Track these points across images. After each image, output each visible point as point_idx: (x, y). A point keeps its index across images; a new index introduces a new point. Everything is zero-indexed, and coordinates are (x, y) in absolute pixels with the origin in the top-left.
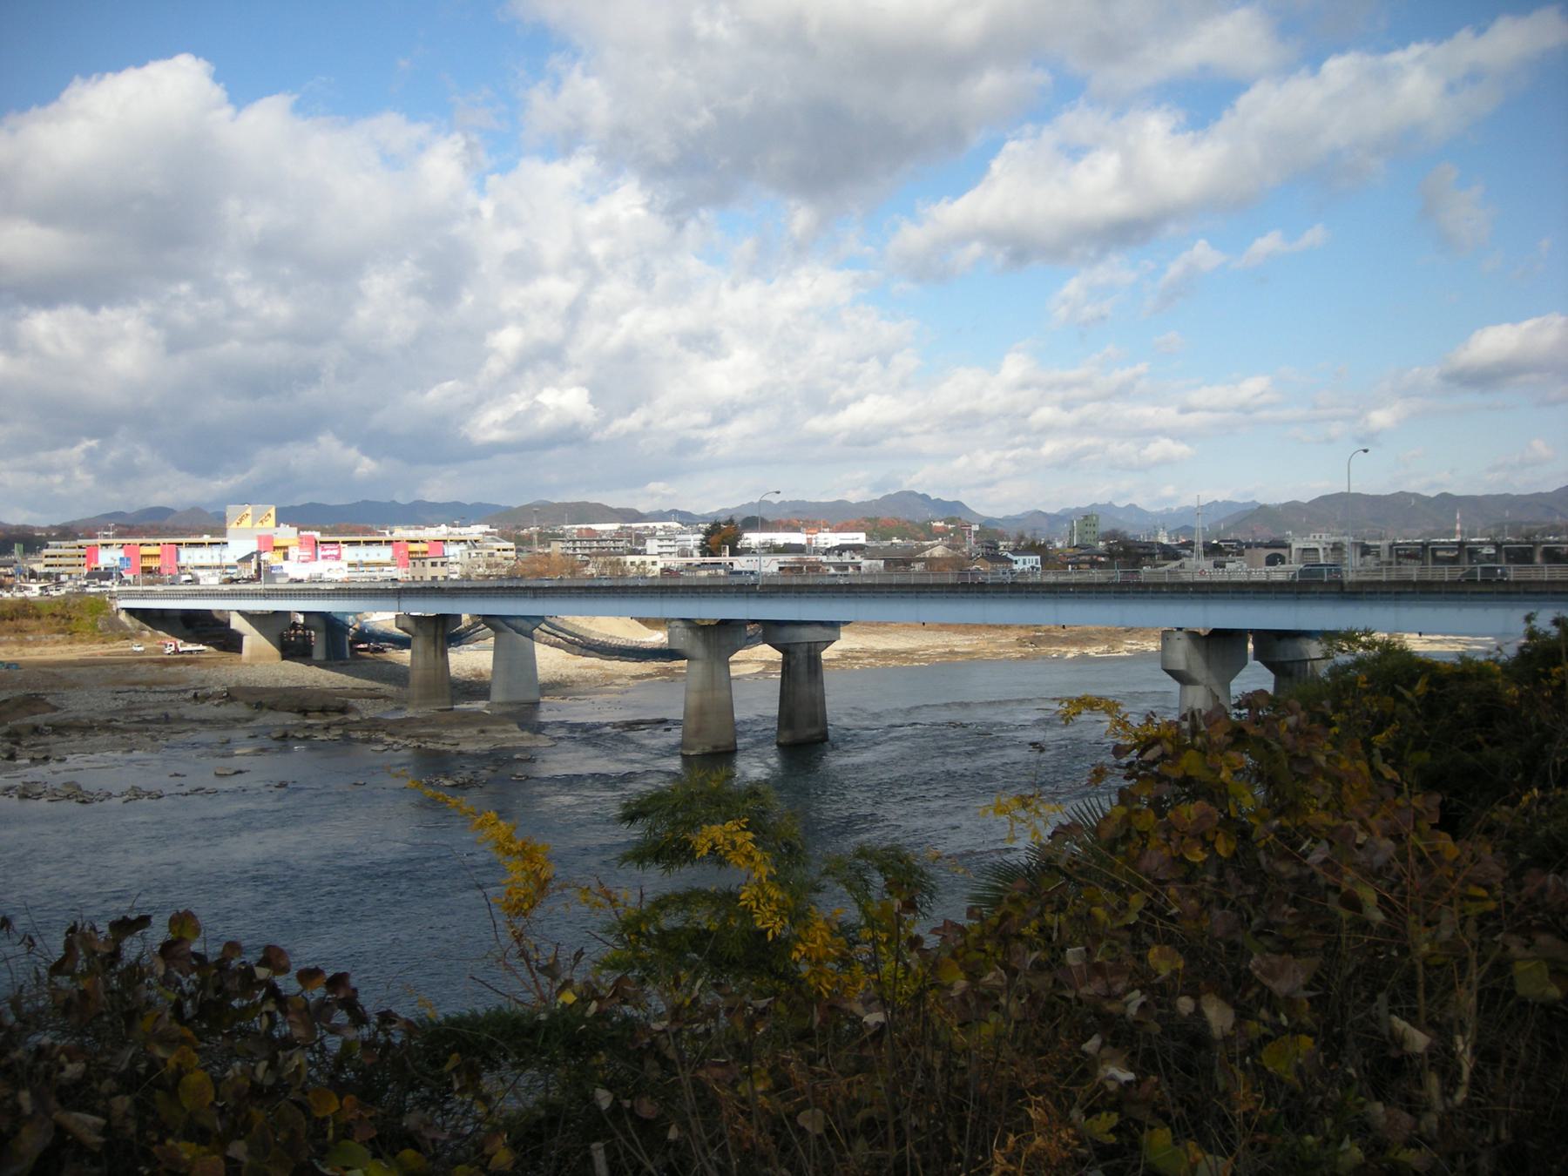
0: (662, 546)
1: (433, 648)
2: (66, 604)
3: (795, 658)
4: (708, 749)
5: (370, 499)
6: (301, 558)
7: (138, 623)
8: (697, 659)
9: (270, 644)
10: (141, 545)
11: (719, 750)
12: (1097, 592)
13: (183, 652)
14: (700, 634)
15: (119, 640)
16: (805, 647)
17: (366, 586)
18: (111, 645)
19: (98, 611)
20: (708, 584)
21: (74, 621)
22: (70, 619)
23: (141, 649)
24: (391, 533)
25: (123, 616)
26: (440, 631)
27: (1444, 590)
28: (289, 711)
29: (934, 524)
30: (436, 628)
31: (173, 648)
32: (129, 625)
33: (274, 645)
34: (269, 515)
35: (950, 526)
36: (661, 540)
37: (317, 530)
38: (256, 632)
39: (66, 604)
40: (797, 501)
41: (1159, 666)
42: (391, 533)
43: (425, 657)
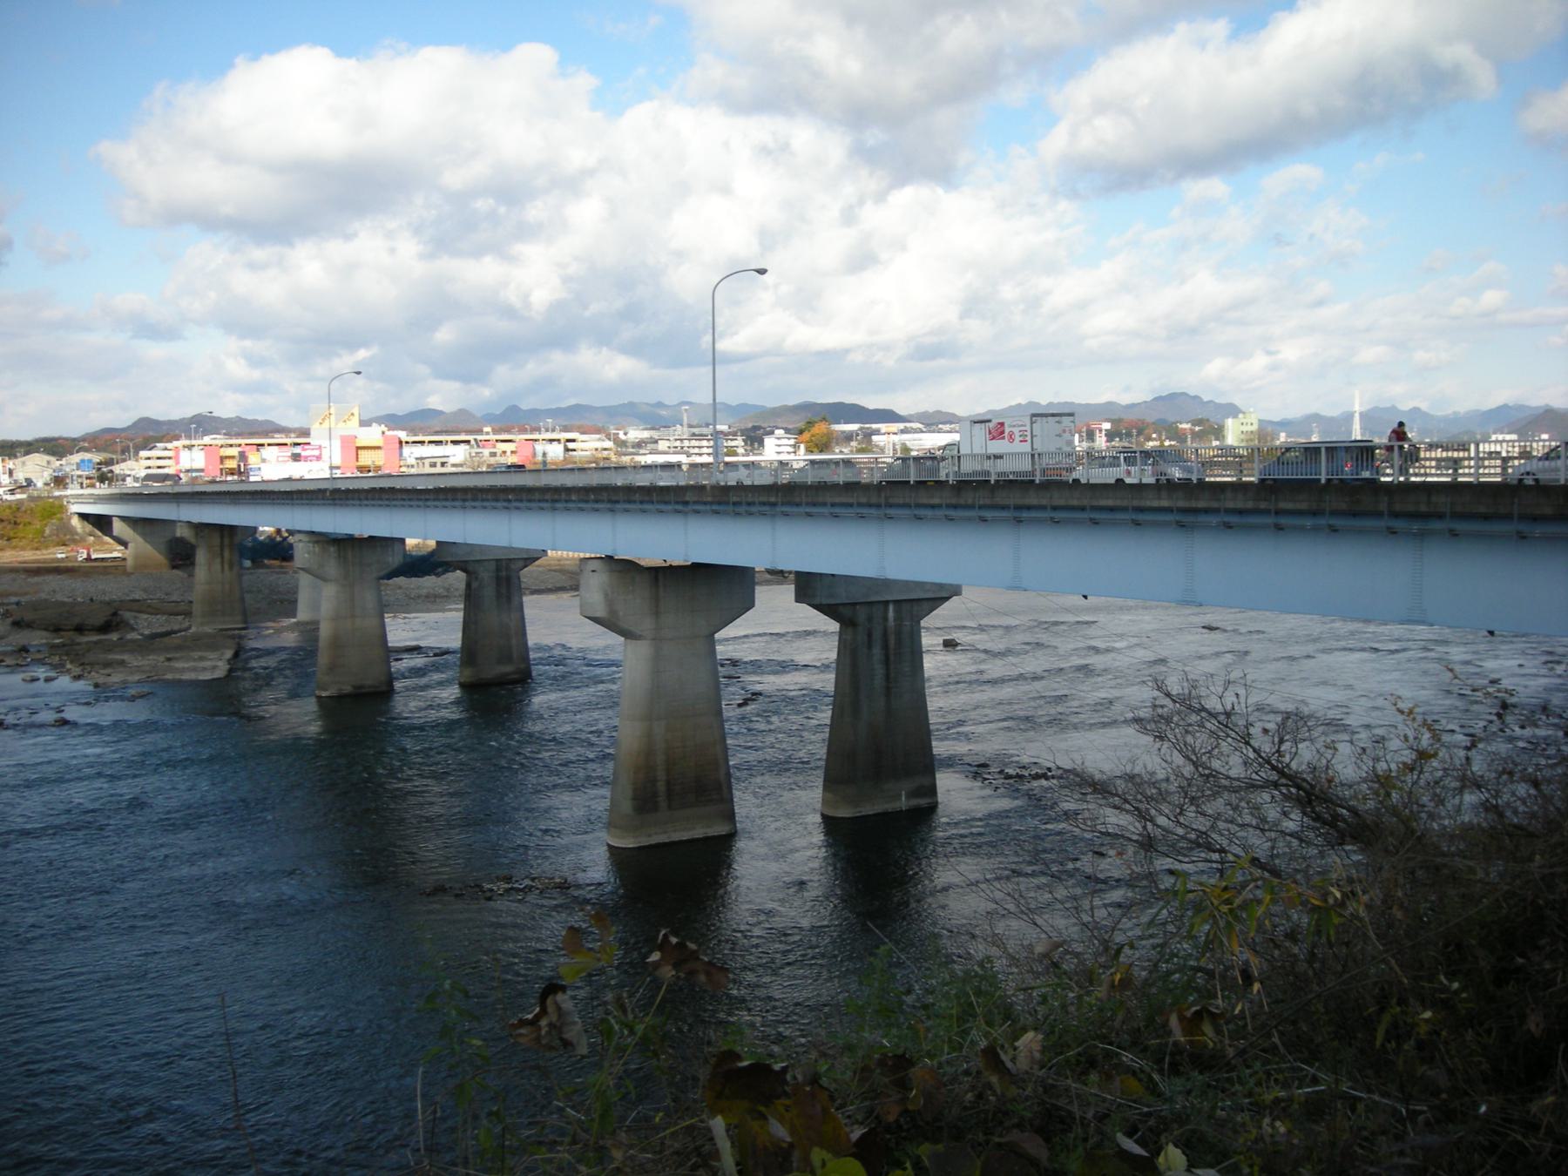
0: (779, 446)
1: (218, 560)
2: (18, 509)
3: (476, 578)
4: (348, 689)
5: (895, 410)
6: (280, 459)
7: (89, 527)
8: (331, 581)
9: (154, 551)
10: (222, 446)
11: (363, 690)
12: (610, 501)
13: (96, 559)
14: (332, 549)
15: (54, 546)
16: (493, 566)
17: (1108, 475)
18: (44, 552)
19: (52, 515)
20: (809, 480)
21: (21, 526)
22: (15, 523)
23: (63, 556)
24: (625, 434)
25: (75, 521)
26: (227, 541)
27: (804, 500)
28: (46, 629)
29: (1180, 426)
30: (222, 537)
31: (85, 556)
32: (79, 530)
33: (160, 553)
34: (352, 414)
35: (1197, 429)
36: (778, 438)
37: (403, 429)
38: (139, 539)
39: (18, 509)
40: (1066, 403)
41: (578, 611)
42: (625, 434)
43: (209, 570)
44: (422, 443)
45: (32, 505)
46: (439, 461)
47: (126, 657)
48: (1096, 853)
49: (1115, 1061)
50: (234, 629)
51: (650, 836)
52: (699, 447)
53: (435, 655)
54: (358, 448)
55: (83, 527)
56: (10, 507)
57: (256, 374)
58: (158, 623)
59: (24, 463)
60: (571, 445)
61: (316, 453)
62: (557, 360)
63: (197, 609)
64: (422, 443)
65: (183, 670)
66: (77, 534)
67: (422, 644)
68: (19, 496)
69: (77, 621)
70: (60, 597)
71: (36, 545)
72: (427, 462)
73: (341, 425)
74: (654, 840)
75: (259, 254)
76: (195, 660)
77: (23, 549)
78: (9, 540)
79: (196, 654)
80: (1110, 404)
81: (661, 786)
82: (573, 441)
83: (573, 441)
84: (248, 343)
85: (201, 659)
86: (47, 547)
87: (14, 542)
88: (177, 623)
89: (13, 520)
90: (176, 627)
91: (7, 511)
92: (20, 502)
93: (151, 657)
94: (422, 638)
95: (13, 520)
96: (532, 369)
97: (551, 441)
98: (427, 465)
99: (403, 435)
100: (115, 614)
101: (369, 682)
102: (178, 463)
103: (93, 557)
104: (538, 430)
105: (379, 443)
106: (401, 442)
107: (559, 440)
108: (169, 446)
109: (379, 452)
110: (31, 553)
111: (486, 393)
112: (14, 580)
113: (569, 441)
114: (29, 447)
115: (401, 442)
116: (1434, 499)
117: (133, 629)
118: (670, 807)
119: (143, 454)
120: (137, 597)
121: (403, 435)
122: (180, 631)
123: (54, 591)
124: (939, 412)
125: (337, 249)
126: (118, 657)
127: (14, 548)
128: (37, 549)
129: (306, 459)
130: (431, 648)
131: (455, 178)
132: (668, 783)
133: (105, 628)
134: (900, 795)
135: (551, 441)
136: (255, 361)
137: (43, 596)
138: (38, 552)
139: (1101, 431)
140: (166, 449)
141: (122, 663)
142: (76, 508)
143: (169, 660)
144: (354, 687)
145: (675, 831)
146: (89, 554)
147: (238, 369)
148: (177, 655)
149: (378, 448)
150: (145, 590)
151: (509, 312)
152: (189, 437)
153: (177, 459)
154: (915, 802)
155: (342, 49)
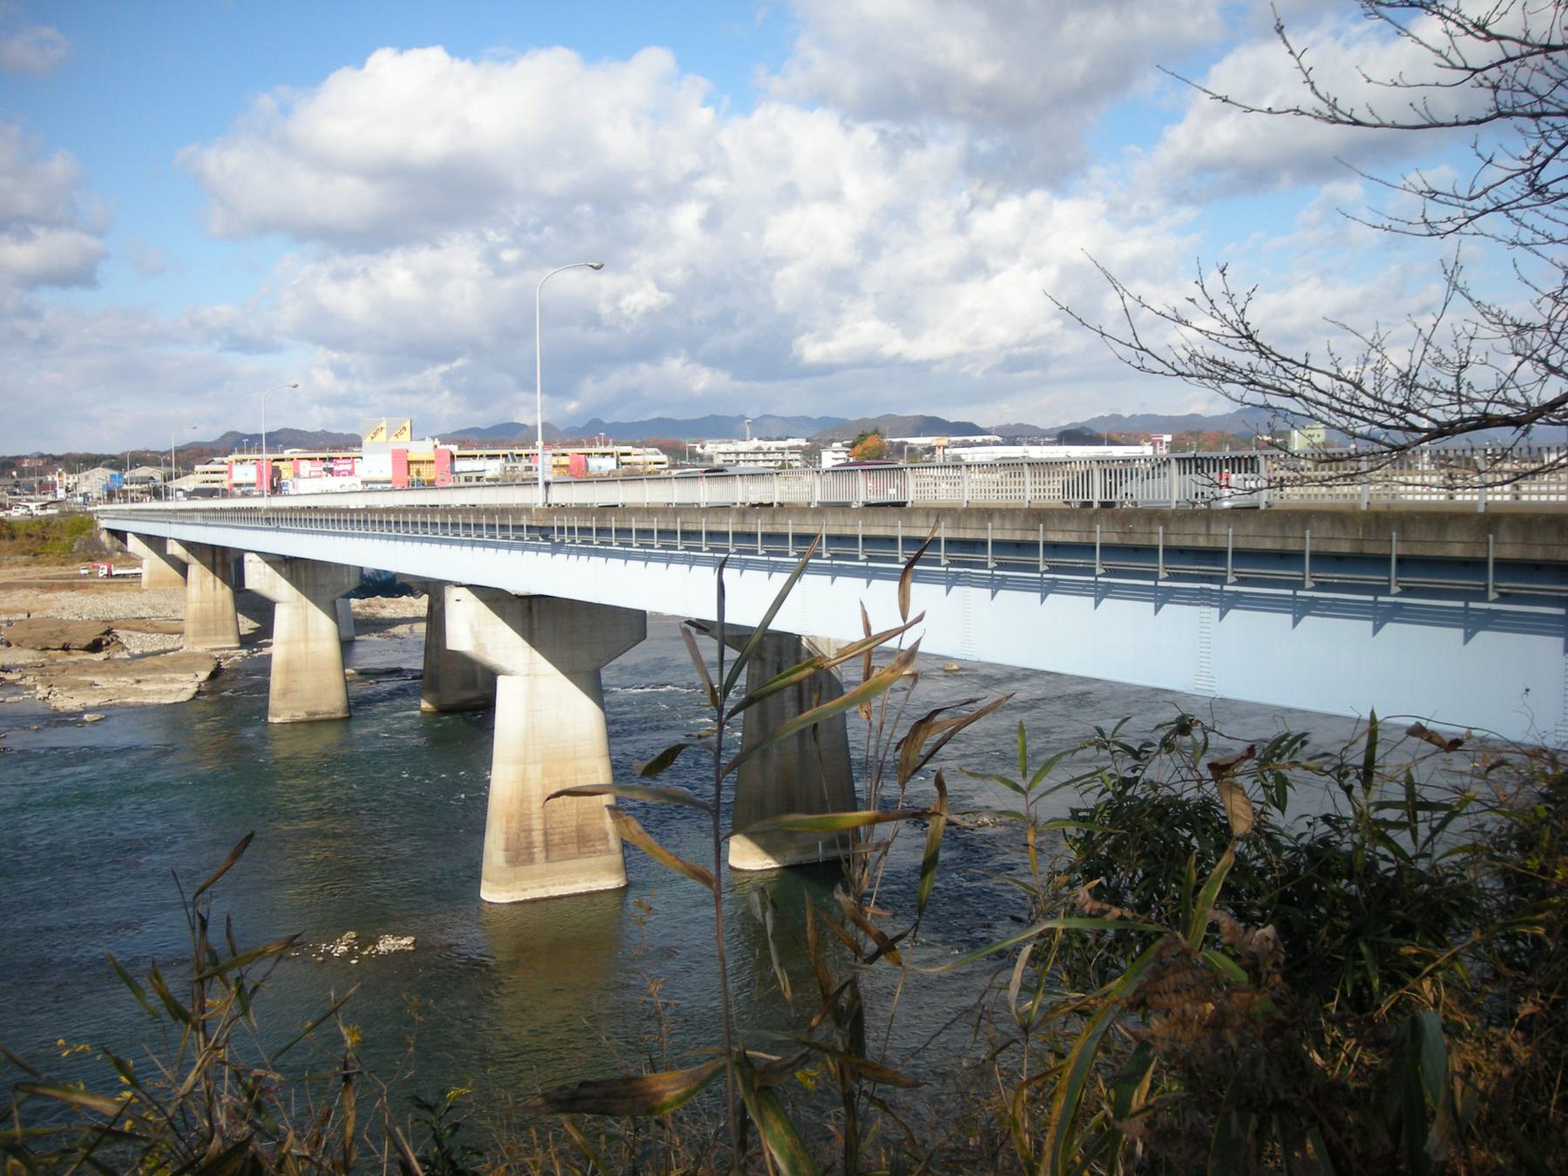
4: (301, 716)
13: (117, 576)
19: (81, 530)
22: (44, 538)
23: (86, 571)
24: (703, 447)
25: (104, 537)
31: (105, 572)
32: (108, 545)
42: (703, 447)
44: (474, 457)
45: (62, 520)
46: (474, 475)
47: (97, 679)
48: (1013, 918)
49: (1386, 972)
50: (224, 649)
51: (525, 890)
52: (755, 461)
53: (413, 678)
54: (409, 463)
55: (112, 543)
56: (40, 522)
57: (342, 388)
58: (153, 642)
59: (87, 477)
60: (625, 459)
61: (349, 467)
62: (645, 370)
63: (189, 627)
64: (474, 457)
65: (149, 693)
66: (105, 549)
67: (404, 666)
68: (49, 512)
69: (65, 639)
70: (66, 616)
71: (62, 560)
72: (462, 476)
73: (393, 439)
74: (528, 896)
75: (343, 263)
76: (165, 682)
77: (48, 564)
78: (35, 555)
79: (167, 676)
80: (1193, 416)
81: (538, 837)
82: (629, 454)
83: (629, 454)
84: (335, 356)
85: (172, 681)
86: (72, 563)
87: (41, 557)
88: (170, 642)
89: (41, 534)
90: (169, 647)
91: (37, 526)
92: (51, 517)
93: (124, 679)
94: (403, 661)
95: (41, 534)
96: (617, 380)
97: (604, 454)
98: (462, 479)
99: (454, 449)
100: (108, 632)
101: (324, 709)
102: (231, 477)
103: (114, 573)
104: (592, 443)
105: (432, 457)
106: (452, 457)
107: (612, 454)
108: (226, 460)
109: (432, 466)
110: (57, 568)
111: (572, 406)
112: (26, 596)
113: (623, 454)
114: (91, 461)
115: (452, 457)
116: (1214, 529)
117: (124, 648)
118: (548, 859)
119: (198, 468)
120: (143, 615)
121: (454, 449)
122: (173, 650)
123: (63, 609)
124: (1021, 425)
125: (425, 257)
126: (89, 679)
127: (40, 563)
128: (63, 564)
129: (338, 473)
130: (412, 671)
131: (555, 182)
132: (546, 834)
133: (95, 647)
134: (817, 846)
135: (604, 454)
136: (341, 372)
137: (50, 613)
138: (64, 568)
139: (1161, 443)
140: (223, 463)
141: (93, 684)
142: (103, 524)
143: (138, 682)
144: (309, 714)
145: (554, 885)
146: (109, 570)
147: (325, 380)
148: (149, 677)
149: (432, 462)
150: (153, 607)
151: (594, 321)
152: (241, 451)
153: (229, 473)
154: (832, 853)
155: (463, 48)
